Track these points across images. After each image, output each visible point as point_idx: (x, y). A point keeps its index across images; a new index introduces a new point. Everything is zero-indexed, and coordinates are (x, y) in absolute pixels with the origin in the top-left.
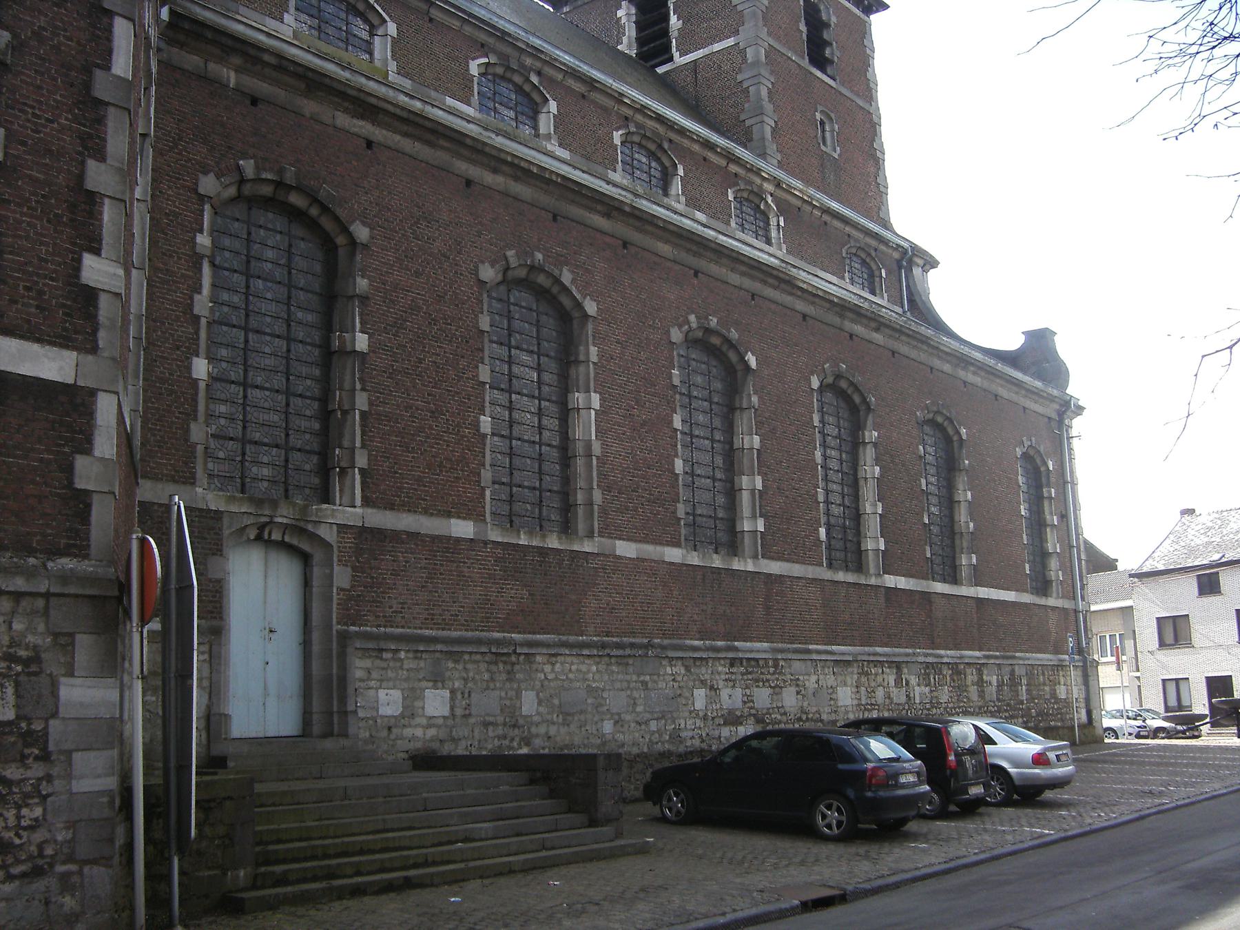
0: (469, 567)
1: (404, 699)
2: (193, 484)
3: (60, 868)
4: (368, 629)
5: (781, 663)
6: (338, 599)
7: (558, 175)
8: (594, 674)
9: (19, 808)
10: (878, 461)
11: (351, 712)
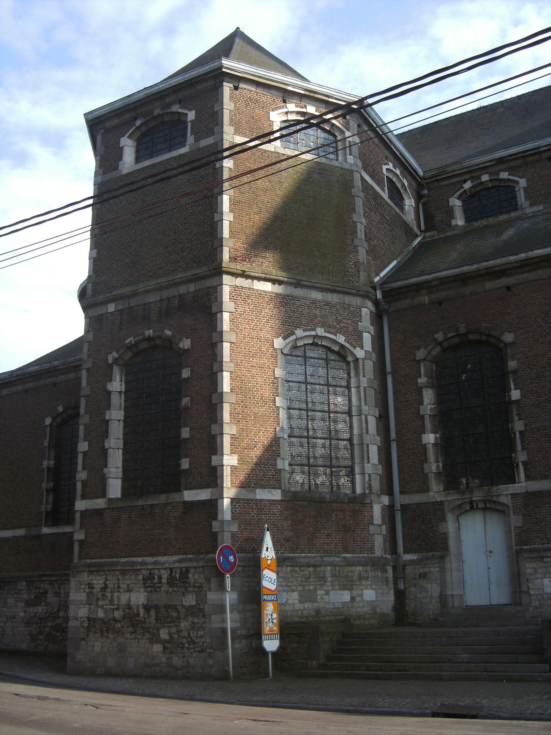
2: (428, 491)
3: (209, 651)
4: (536, 546)
6: (515, 533)
9: (197, 631)
11: (525, 592)
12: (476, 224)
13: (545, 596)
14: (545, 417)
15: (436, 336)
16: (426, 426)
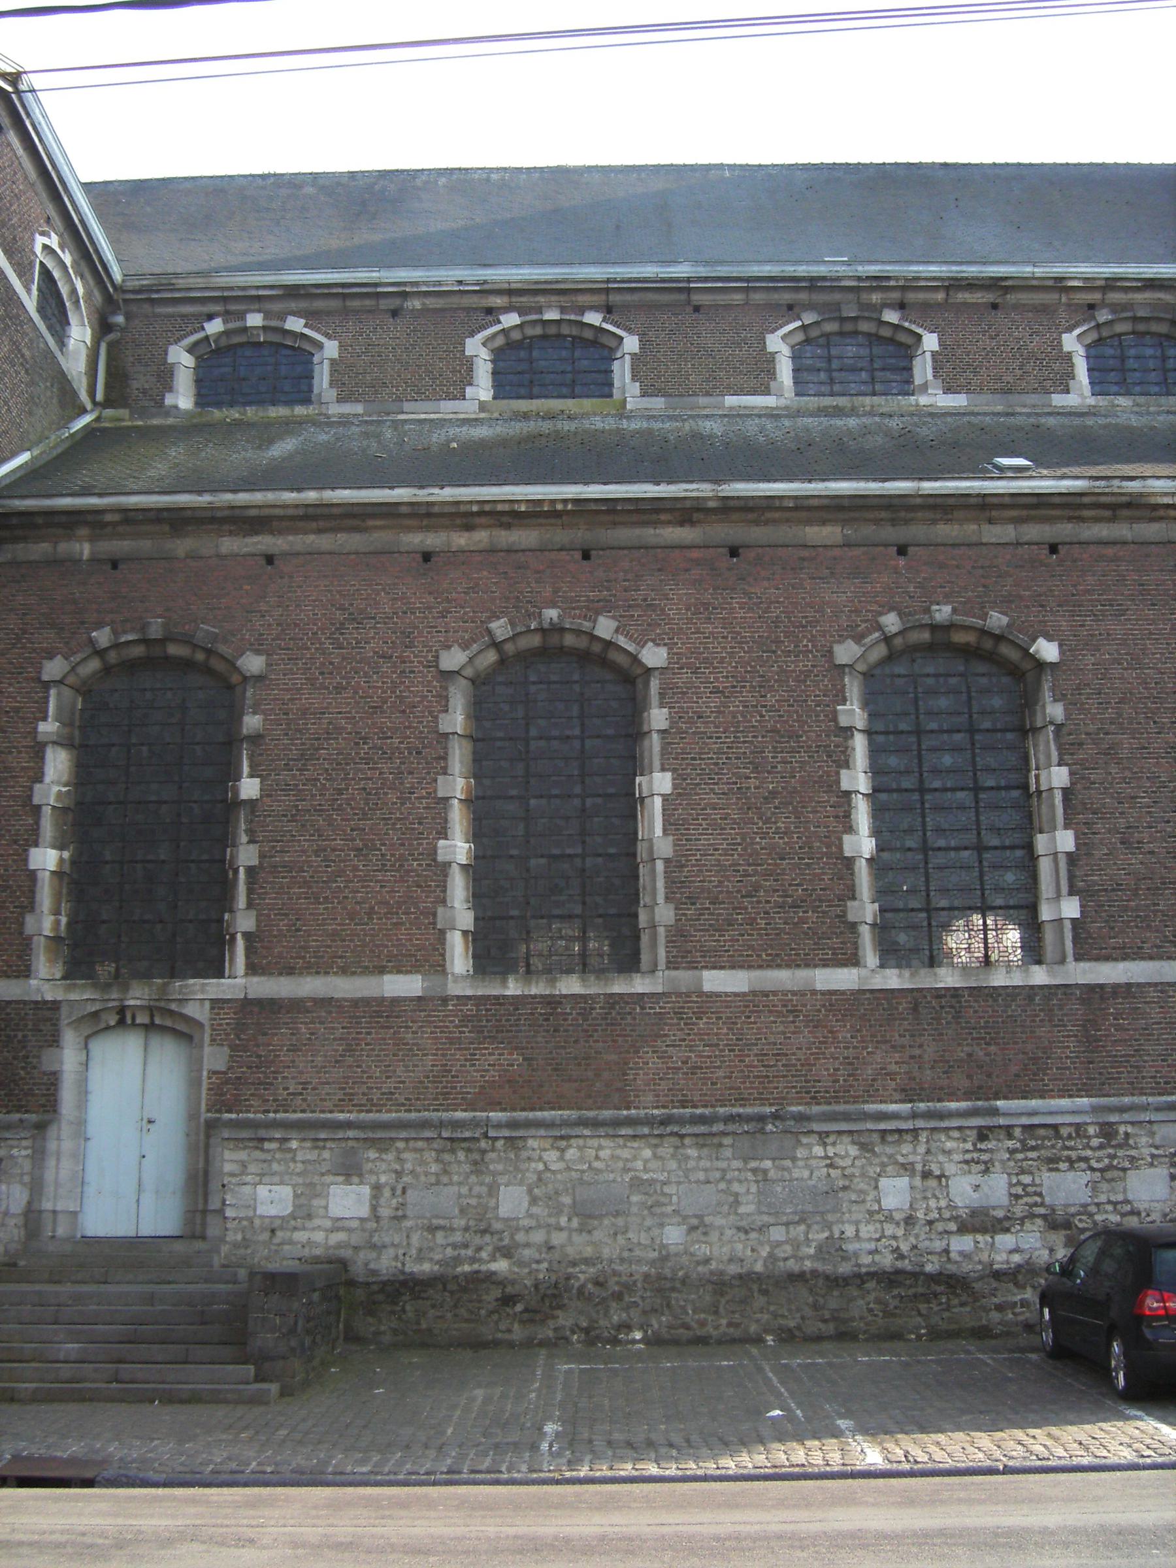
0: (413, 1033)
1: (296, 1196)
2: (28, 976)
4: (251, 1116)
8: (646, 1161)
12: (217, 414)
13: (257, 1222)
14: (307, 844)
15: (94, 634)
16: (42, 830)
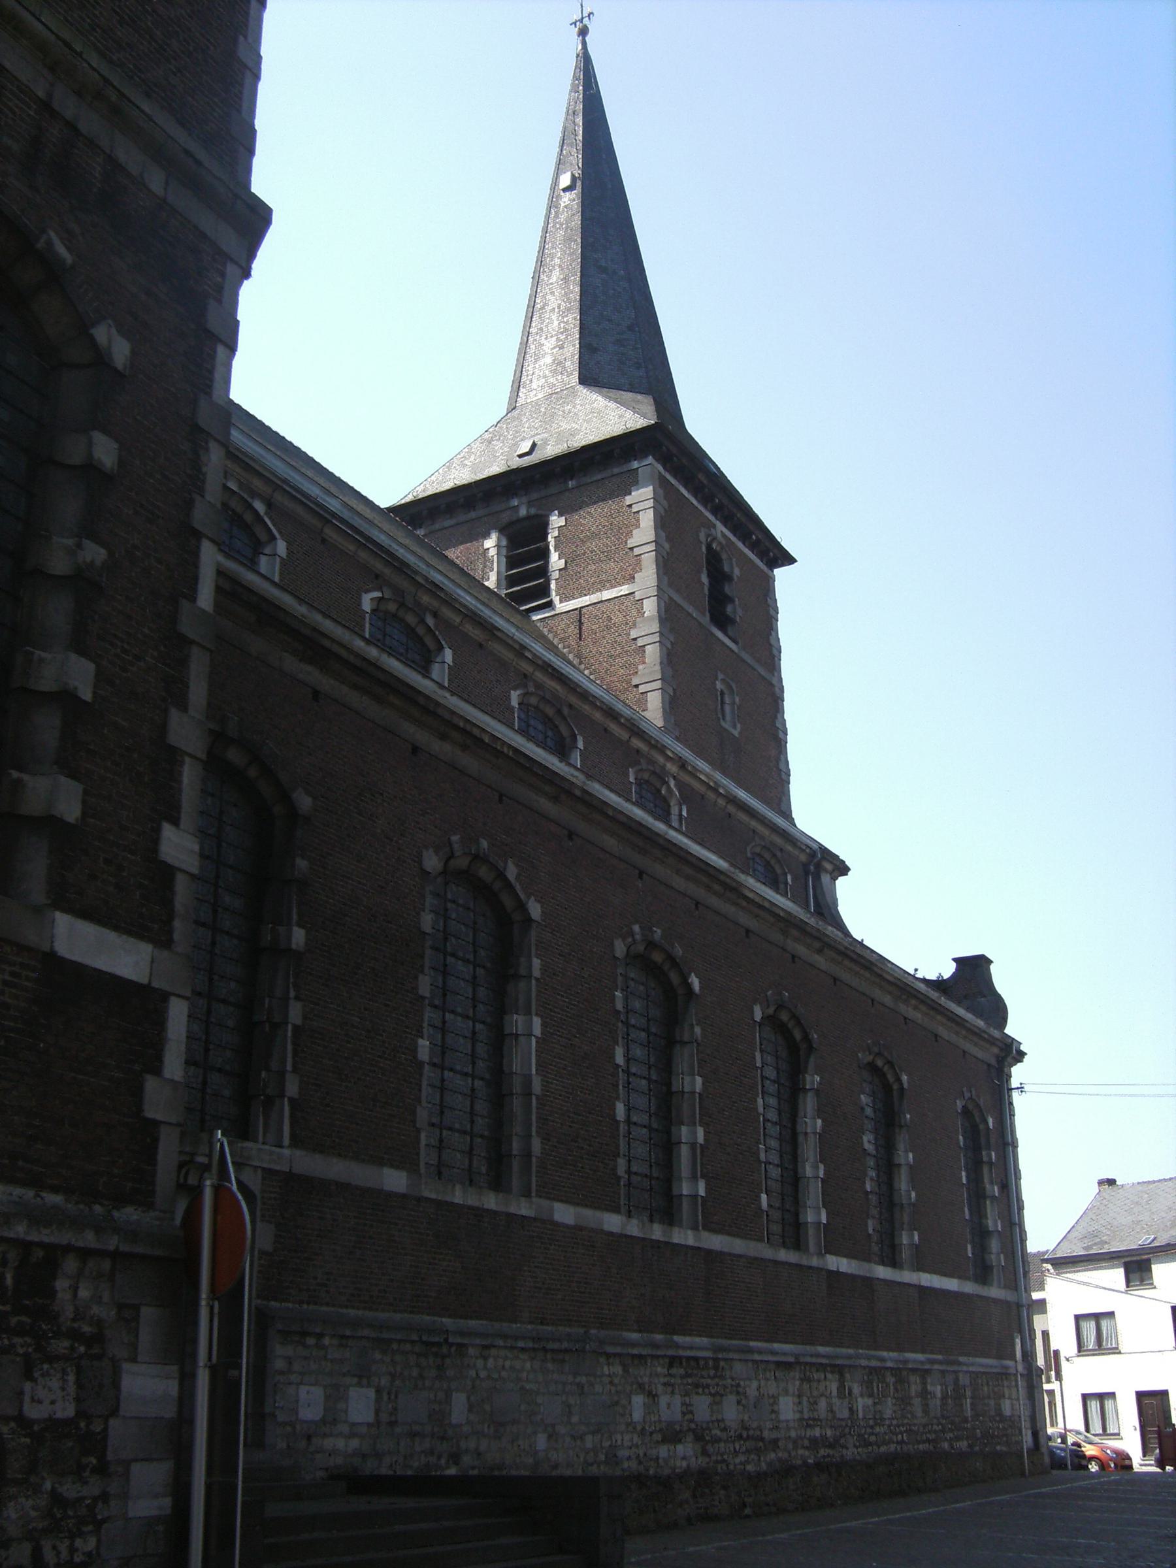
5: (722, 1364)
7: (510, 746)
9: (72, 1537)
10: (820, 1112)
